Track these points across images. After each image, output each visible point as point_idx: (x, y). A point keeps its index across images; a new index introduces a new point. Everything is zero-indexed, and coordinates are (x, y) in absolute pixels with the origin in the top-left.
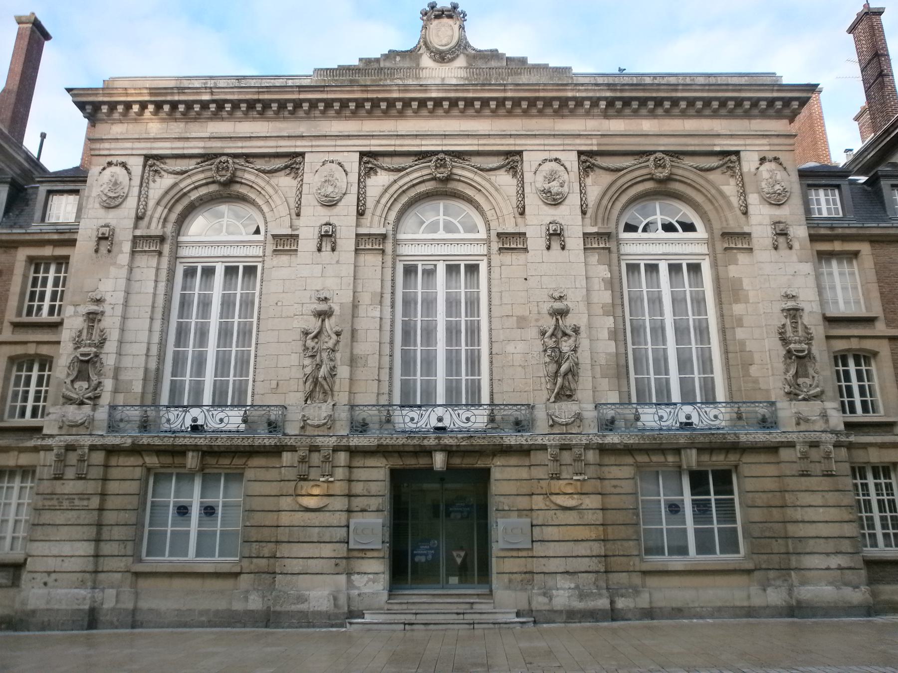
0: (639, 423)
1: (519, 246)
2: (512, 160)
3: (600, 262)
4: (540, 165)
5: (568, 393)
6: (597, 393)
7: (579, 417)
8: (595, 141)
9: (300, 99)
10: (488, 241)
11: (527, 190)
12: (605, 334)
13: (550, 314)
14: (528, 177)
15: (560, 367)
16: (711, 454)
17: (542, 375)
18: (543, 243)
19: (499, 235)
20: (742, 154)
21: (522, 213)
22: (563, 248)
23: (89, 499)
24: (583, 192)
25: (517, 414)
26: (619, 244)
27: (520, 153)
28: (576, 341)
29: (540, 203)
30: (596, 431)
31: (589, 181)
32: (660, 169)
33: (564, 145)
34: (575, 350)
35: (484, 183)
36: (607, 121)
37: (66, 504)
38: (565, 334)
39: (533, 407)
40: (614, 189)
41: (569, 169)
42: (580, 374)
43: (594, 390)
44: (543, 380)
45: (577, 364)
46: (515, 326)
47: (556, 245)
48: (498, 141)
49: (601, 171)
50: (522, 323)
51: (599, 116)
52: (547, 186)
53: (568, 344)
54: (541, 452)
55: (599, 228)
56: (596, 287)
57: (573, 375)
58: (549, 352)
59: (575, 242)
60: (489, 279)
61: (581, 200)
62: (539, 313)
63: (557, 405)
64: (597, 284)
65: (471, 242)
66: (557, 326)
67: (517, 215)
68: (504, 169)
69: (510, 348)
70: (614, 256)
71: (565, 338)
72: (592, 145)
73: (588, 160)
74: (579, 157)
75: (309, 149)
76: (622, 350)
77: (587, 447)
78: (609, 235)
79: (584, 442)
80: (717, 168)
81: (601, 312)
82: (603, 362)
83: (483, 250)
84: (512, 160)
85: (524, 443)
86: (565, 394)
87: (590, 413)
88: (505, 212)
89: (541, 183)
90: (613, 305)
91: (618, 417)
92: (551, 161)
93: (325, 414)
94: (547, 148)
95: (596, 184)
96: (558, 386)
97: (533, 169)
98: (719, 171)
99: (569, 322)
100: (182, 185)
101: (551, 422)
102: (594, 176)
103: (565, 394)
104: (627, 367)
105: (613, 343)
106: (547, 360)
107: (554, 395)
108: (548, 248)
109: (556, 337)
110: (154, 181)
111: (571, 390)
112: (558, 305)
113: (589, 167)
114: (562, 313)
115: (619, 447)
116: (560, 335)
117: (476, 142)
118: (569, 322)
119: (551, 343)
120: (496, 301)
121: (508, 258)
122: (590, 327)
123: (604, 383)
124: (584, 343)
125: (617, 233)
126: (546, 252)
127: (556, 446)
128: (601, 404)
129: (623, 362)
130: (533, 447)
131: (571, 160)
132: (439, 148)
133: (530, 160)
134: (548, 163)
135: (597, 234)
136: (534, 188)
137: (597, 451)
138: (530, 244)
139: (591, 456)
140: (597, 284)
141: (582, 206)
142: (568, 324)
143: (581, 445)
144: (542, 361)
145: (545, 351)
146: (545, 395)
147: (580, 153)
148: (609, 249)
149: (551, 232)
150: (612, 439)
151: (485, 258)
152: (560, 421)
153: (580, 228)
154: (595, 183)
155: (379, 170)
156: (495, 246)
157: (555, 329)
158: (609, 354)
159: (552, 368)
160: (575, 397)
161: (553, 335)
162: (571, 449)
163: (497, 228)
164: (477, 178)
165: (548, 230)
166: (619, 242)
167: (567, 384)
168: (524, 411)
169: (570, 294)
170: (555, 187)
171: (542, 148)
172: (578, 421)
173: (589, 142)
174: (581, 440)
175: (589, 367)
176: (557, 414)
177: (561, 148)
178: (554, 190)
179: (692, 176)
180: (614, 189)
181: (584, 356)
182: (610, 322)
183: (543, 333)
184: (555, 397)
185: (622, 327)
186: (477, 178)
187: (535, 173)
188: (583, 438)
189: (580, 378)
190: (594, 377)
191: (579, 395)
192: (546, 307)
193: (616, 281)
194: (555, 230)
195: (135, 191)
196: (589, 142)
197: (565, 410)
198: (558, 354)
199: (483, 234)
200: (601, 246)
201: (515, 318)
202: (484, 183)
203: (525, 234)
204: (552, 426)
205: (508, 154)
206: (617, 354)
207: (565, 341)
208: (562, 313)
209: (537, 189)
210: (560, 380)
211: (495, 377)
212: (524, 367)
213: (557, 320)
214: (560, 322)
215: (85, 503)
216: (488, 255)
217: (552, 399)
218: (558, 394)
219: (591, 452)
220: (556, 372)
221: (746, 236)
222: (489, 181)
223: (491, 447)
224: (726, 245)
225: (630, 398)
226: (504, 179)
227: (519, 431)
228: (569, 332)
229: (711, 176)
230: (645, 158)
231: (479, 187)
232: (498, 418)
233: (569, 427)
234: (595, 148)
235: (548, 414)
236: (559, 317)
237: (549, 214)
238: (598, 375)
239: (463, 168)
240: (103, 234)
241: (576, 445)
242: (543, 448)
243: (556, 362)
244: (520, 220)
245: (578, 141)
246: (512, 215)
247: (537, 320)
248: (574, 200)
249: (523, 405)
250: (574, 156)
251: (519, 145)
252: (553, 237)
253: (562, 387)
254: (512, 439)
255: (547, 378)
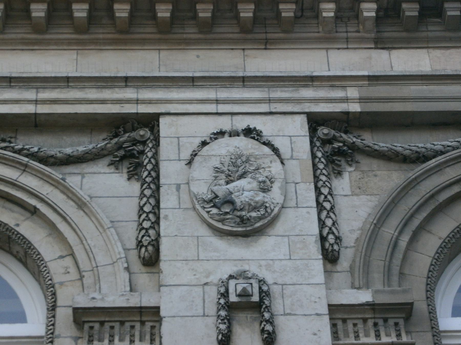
2: (130, 142)
4: (204, 144)
8: (353, 93)
11: (168, 200)
14: (171, 170)
21: (152, 261)
24: (324, 205)
27: (151, 122)
29: (203, 231)
31: (343, 185)
33: (270, 101)
35: (45, 190)
36: (384, 54)
40: (412, 200)
41: (285, 150)
48: (92, 94)
49: (375, 163)
51: (362, 40)
52: (222, 190)
55: (376, 292)
61: (322, 224)
67: (137, 266)
68: (107, 160)
72: (346, 100)
73: (338, 140)
74: (313, 130)
78: (406, 311)
84: (130, 142)
88: (101, 259)
89: (202, 180)
92: (234, 134)
94: (222, 108)
95: (358, 199)
97: (186, 155)
102: (357, 175)
113: (339, 153)
117: (30, 95)
125: (432, 312)
131: (292, 134)
133: (176, 136)
134: (226, 140)
135: (372, 307)
136: (185, 196)
141: (323, 239)
147: (315, 121)
149: (233, 298)
153: (322, 292)
154: (358, 190)
163: (72, 297)
164: (29, 181)
165: (225, 295)
170: (245, 190)
171: (212, 108)
173: (340, 94)
177: (264, 108)
178: (241, 199)
180: (412, 200)
186: (29, 181)
187: (190, 163)
194: (244, 294)
196: (340, 94)
202: (45, 190)
203: (156, 310)
205: (118, 124)
209: (193, 196)
226: (109, 186)
229: (74, 178)
231: (33, 202)
234: (355, 108)
237: (227, 258)
244: (143, 278)
245: (307, 93)
246: (122, 265)
248: (302, 221)
250: (298, 127)
251: (150, 102)
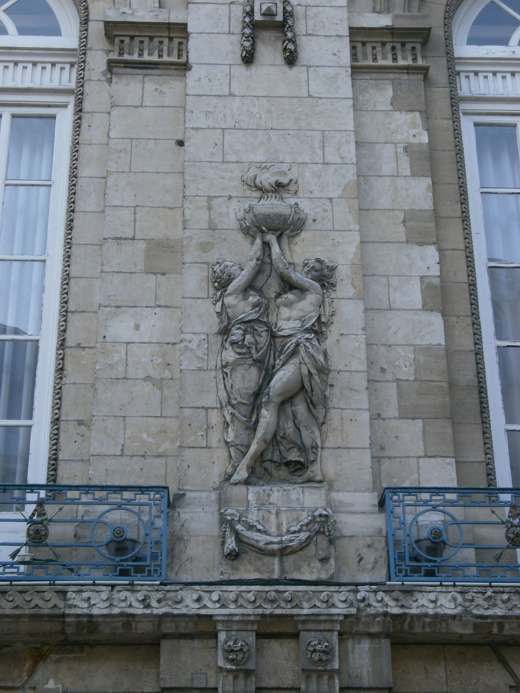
1: (166, 58)
3: (397, 105)
5: (294, 456)
6: (386, 465)
7: (323, 529)
10: (79, 57)
12: (414, 295)
13: (246, 231)
15: (268, 375)
17: (211, 401)
18: (231, 46)
19: (112, 29)
22: (291, 59)
25: (116, 517)
26: (453, 76)
28: (321, 304)
30: (380, 575)
34: (318, 329)
38: (289, 285)
39: (180, 497)
42: (334, 402)
43: (379, 454)
44: (215, 418)
45: (323, 371)
46: (141, 266)
47: (269, 52)
50: (162, 257)
53: (295, 313)
54: (196, 643)
55: (396, 17)
56: (387, 168)
57: (311, 404)
58: (236, 334)
59: (326, 47)
60: (76, 145)
62: (212, 227)
63: (252, 493)
64: (389, 161)
65: (36, 57)
66: (264, 264)
69: (121, 328)
70: (440, 95)
71: (290, 296)
76: (466, 342)
77: (350, 628)
78: (423, 35)
79: (341, 609)
81: (401, 232)
82: (407, 373)
83: (66, 79)
85: (138, 610)
86: (284, 460)
87: (358, 517)
90: (436, 215)
91: (452, 535)
96: (259, 434)
99: (300, 253)
101: (231, 544)
103: (284, 460)
104: (482, 390)
105: (436, 320)
106: (230, 355)
107: (246, 461)
108: (248, 59)
109: (260, 292)
111: (302, 449)
112: (270, 206)
114: (286, 228)
115: (458, 629)
116: (273, 287)
118: (300, 253)
119: (242, 307)
120: (87, 202)
121: (131, 88)
122: (365, 272)
123: (410, 436)
124: (348, 310)
126: (240, 70)
127: (244, 622)
128: (395, 490)
129: (468, 376)
130: (168, 627)
135: (391, 31)
137: (386, 644)
138: (197, 49)
139: (364, 661)
140: (389, 161)
142: (298, 260)
143: (330, 619)
144: (214, 361)
145: (225, 332)
146: (217, 462)
148: (425, 71)
149: (258, 17)
150: (437, 601)
151: (71, 100)
152: (261, 539)
153: (343, 14)
156: (97, 61)
157: (258, 272)
158: (427, 349)
159: (247, 379)
160: (315, 471)
161: (250, 287)
162: (296, 636)
165: (250, 14)
166: (453, 67)
167: (289, 428)
168: (149, 508)
169: (308, 179)
172: (322, 541)
174: (329, 603)
175: (360, 381)
176: (253, 518)
181: (347, 350)
182: (427, 260)
183: (221, 283)
184: (252, 470)
185: (463, 277)
188: (337, 598)
189: (334, 414)
190: (376, 417)
191: (327, 464)
192: (232, 213)
193: (446, 157)
194: (269, 13)
197: (281, 510)
198: (264, 339)
199: (69, 38)
200: (401, 62)
201: (142, 245)
204: (233, 556)
206: (449, 352)
207: (289, 305)
208: (286, 228)
210: (267, 416)
211: (70, 412)
212: (159, 384)
213: (266, 245)
214: (275, 249)
216: (79, 95)
217: (242, 474)
218: (260, 457)
219: (366, 645)
220: (257, 394)
223: (25, 627)
225: (490, 473)
227: (124, 573)
228: (299, 276)
232: (56, 532)
233: (290, 560)
235: (223, 520)
236: (272, 238)
238: (392, 411)
241: (313, 618)
242: (203, 629)
243: (258, 362)
247: (205, 247)
249: (142, 489)
252: (265, 35)
253: (275, 440)
254: (96, 600)
255: (228, 411)
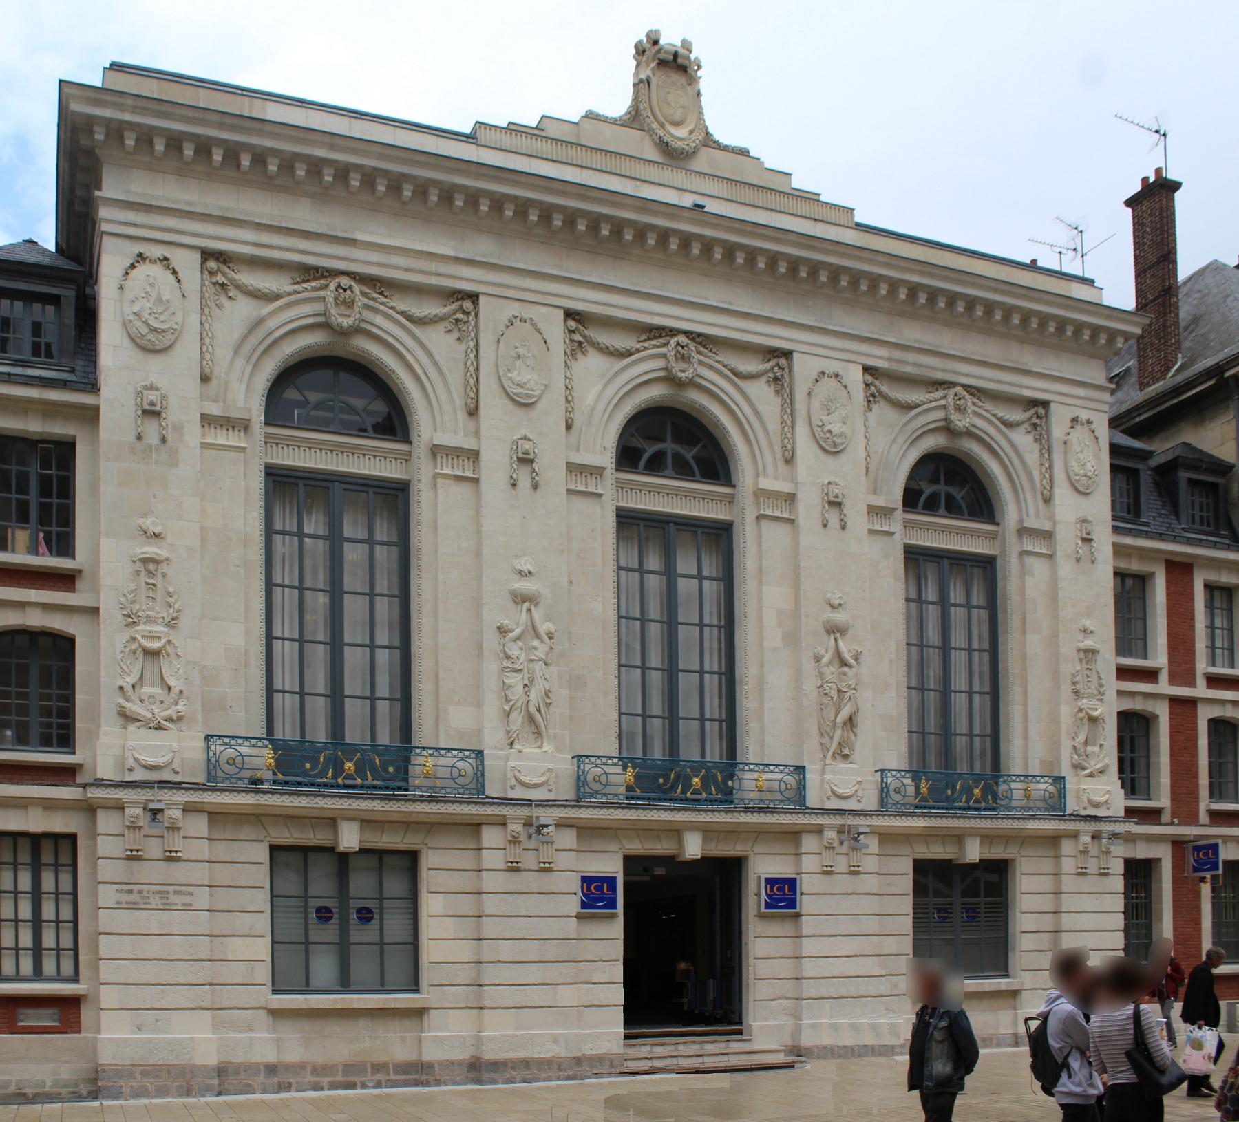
0: (730, 783)
9: (122, 122)
16: (991, 845)
20: (1053, 406)
23: (191, 894)
31: (872, 416)
32: (343, 310)
37: (155, 901)
75: (490, 290)
80: (1023, 423)
93: (619, 770)
98: (441, 327)
100: (272, 323)
110: (219, 306)
132: (341, 265)
155: (590, 350)
179: (992, 431)
195: (194, 319)
205: (1034, 403)
213: (836, 640)
215: (187, 899)
221: (1047, 536)
222: (742, 393)
224: (572, 487)
226: (441, 341)
229: (746, 385)
230: (940, 393)
236: (838, 635)
239: (711, 367)
240: (152, 404)
